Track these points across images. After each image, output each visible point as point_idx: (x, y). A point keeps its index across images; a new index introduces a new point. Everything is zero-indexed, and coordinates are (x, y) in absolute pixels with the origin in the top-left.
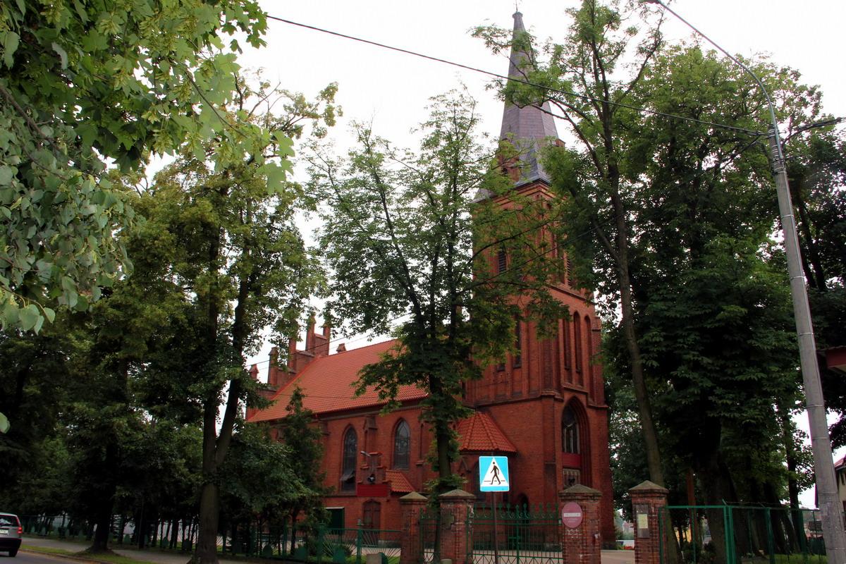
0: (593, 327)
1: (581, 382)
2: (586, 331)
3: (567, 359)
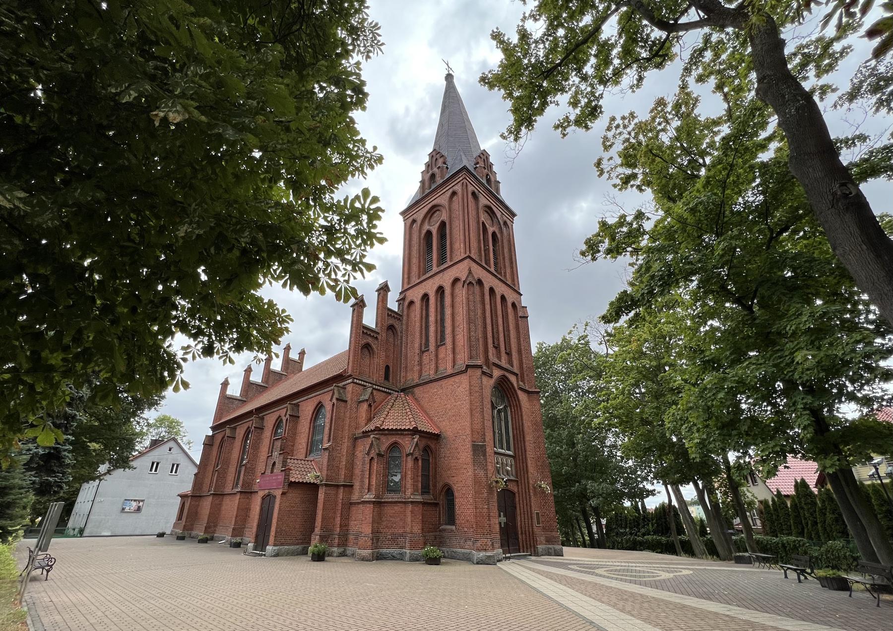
0: (520, 314)
1: (510, 362)
2: (514, 321)
3: (495, 338)
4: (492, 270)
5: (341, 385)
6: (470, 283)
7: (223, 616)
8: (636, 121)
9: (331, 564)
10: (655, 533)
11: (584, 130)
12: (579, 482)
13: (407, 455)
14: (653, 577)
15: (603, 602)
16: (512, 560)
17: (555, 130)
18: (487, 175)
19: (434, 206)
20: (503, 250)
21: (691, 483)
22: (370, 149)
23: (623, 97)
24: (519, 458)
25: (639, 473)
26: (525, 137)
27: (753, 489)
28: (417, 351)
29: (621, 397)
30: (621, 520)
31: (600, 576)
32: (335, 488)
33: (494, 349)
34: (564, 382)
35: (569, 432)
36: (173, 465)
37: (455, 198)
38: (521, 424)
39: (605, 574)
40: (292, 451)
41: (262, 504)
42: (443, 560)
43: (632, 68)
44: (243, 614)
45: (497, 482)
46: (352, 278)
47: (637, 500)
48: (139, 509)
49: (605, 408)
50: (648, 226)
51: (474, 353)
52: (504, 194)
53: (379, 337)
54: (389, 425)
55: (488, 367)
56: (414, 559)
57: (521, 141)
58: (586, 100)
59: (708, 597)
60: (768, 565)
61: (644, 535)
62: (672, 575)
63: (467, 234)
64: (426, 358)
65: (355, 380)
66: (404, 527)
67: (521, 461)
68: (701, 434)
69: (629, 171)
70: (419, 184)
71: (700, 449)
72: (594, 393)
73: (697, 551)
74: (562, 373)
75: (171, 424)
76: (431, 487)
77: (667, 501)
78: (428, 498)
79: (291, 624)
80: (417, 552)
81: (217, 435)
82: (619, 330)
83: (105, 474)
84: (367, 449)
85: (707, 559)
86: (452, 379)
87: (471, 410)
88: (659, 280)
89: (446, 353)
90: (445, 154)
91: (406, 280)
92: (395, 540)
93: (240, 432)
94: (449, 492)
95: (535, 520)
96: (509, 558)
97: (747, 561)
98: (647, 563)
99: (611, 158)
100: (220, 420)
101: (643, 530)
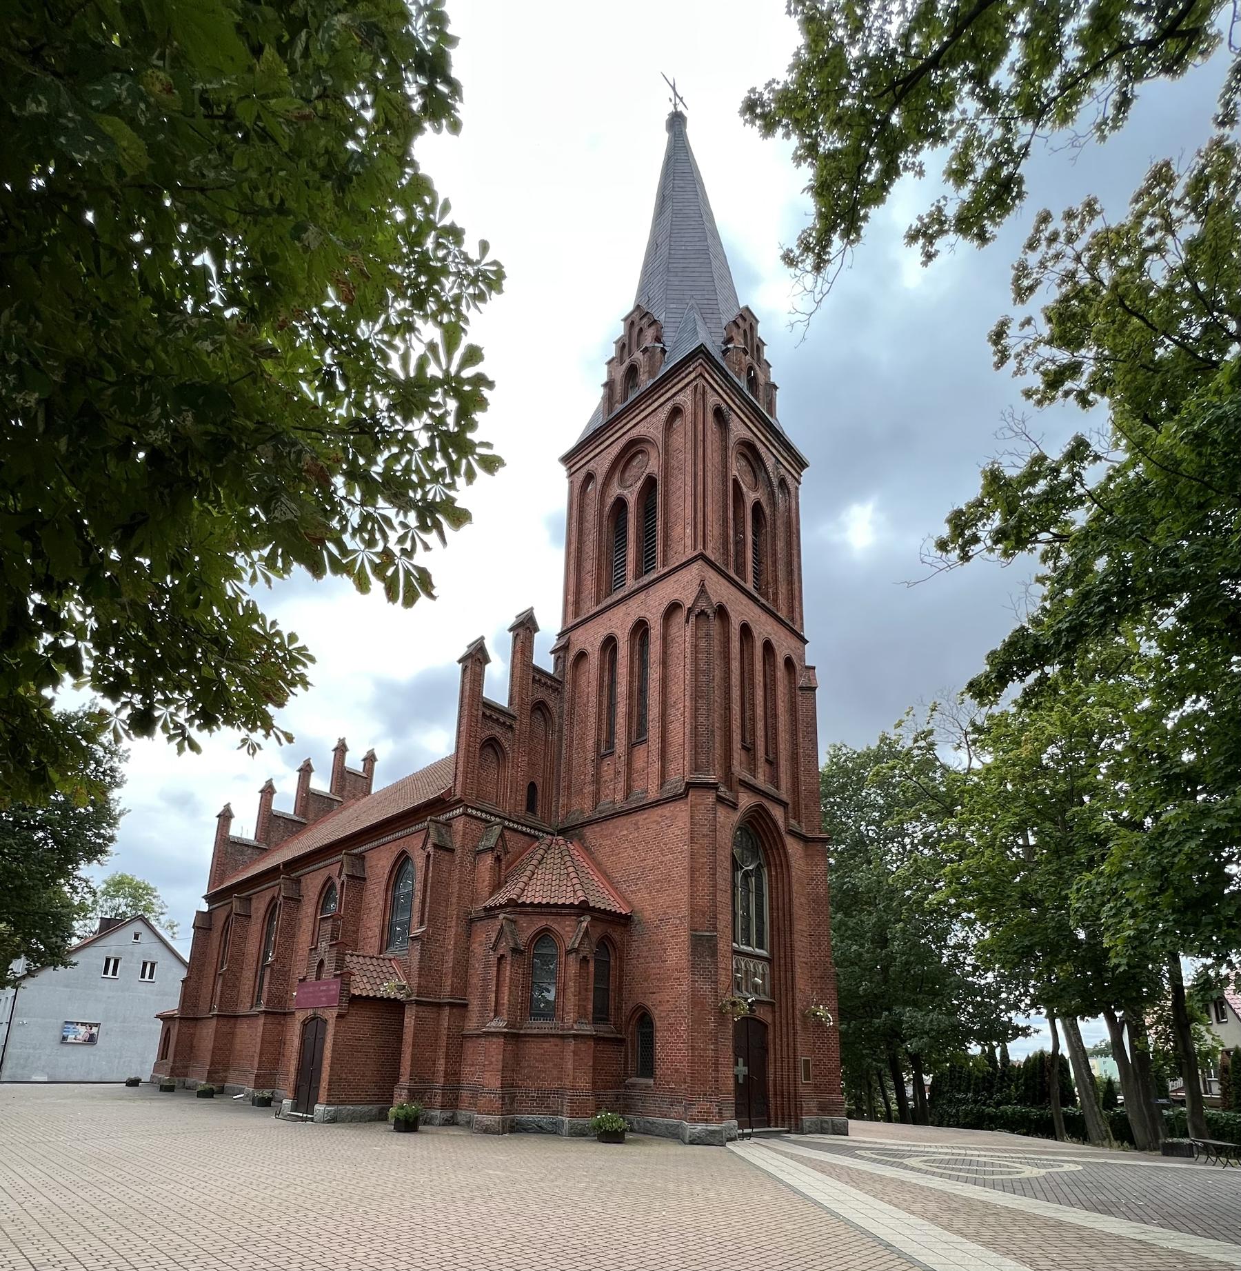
0: (801, 682)
1: (774, 779)
4: (749, 586)
5: (442, 818)
6: (702, 613)
7: (228, 1216)
8: (1097, 225)
9: (430, 1137)
10: (1021, 1101)
11: (976, 243)
12: (889, 1010)
13: (568, 952)
14: (1010, 1173)
15: (912, 1213)
16: (753, 1140)
17: (909, 244)
18: (751, 368)
19: (633, 443)
20: (774, 544)
21: (1101, 1015)
22: (474, 255)
23: (1074, 159)
24: (780, 963)
25: (1004, 995)
26: (838, 261)
27: (1217, 1029)
28: (591, 755)
29: (988, 852)
30: (960, 1078)
31: (913, 1169)
32: (435, 1010)
33: (743, 752)
34: (878, 824)
35: (880, 919)
36: (145, 964)
37: (678, 422)
38: (787, 900)
39: (923, 1166)
40: (355, 942)
41: (303, 1033)
42: (628, 1136)
43: (1106, 73)
44: (264, 1215)
45: (734, 1004)
46: (419, 546)
47: (995, 1043)
48: (91, 1040)
49: (953, 872)
50: (1093, 476)
51: (703, 759)
52: (786, 417)
53: (516, 726)
54: (534, 896)
55: (730, 788)
56: (578, 1133)
57: (830, 269)
58: (988, 163)
59: (1106, 1209)
60: (1224, 1159)
61: (998, 1104)
62: (1043, 1172)
63: (700, 504)
64: (607, 768)
65: (469, 811)
66: (560, 1079)
67: (783, 968)
68: (1139, 920)
69: (1063, 356)
70: (600, 392)
71: (1133, 948)
72: (933, 846)
73: (1093, 1133)
74: (874, 806)
75: (137, 892)
76: (612, 1011)
77: (1049, 1048)
78: (605, 1030)
79: (348, 1232)
80: (581, 1121)
81: (216, 912)
82: (1001, 721)
83: (24, 977)
84: (493, 940)
85: (1111, 1146)
86: (659, 811)
87: (693, 870)
88: (1099, 603)
89: (648, 757)
90: (661, 317)
91: (571, 609)
92: (542, 1100)
93: (259, 907)
94: (644, 1020)
95: (802, 1072)
96: (749, 1136)
97: (1185, 1152)
98: (1000, 1150)
99: (1028, 321)
100: (222, 883)
101: (998, 1096)
